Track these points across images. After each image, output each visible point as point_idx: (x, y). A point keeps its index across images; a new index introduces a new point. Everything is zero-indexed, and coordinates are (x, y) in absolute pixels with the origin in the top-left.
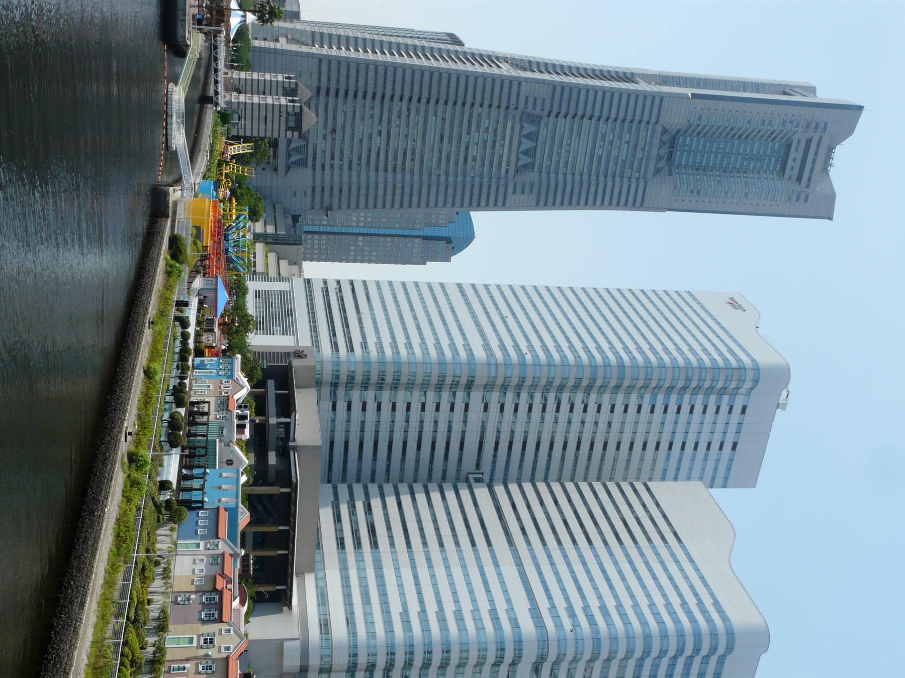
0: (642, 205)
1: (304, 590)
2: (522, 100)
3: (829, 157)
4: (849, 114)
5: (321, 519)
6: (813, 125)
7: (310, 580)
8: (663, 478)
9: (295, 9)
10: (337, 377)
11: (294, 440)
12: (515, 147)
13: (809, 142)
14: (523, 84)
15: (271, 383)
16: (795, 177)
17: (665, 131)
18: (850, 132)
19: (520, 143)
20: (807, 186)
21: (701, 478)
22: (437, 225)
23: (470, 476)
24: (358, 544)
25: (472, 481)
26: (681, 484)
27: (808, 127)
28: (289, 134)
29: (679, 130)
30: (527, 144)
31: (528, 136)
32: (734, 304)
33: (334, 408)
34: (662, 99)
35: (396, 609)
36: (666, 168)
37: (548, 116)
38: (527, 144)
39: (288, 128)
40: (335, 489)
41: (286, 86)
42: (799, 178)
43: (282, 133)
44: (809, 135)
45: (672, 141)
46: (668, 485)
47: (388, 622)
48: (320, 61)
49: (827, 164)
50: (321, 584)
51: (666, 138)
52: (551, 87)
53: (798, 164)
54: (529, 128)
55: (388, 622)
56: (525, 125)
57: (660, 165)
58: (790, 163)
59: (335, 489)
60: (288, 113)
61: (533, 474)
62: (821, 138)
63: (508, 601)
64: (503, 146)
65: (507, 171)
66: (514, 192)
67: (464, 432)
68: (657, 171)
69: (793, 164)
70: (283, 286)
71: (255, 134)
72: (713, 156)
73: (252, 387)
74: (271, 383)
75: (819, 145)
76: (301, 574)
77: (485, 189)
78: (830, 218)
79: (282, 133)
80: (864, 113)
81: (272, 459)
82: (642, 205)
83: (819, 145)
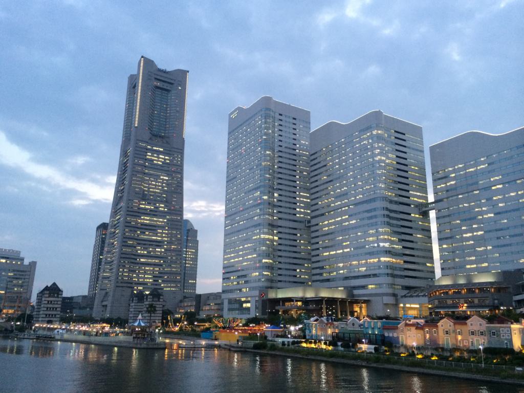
0: (181, 150)
6: (150, 77)
9: (81, 298)
18: (153, 61)
20: (175, 80)
23: (307, 225)
27: (150, 79)
28: (161, 300)
29: (150, 133)
33: (280, 281)
39: (159, 301)
41: (136, 301)
42: (172, 84)
43: (161, 303)
44: (153, 79)
48: (117, 286)
49: (165, 72)
57: (165, 142)
58: (165, 87)
60: (153, 301)
62: (155, 74)
68: (167, 142)
69: (166, 86)
71: (161, 315)
72: (161, 119)
79: (161, 303)
80: (189, 76)
82: (181, 150)
83: (157, 75)
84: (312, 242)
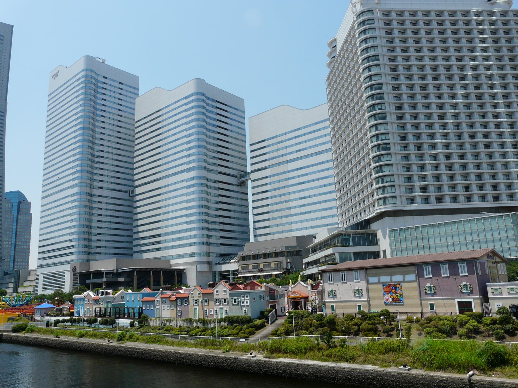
0: (3, 112)
1: (177, 264)
5: (148, 258)
7: (173, 262)
8: (134, 114)
10: (85, 252)
11: (113, 270)
15: (87, 281)
21: (134, 99)
22: (12, 208)
24: (159, 242)
25: (133, 195)
26: (137, 107)
32: (55, 76)
35: (185, 226)
40: (135, 252)
46: (137, 112)
47: (190, 230)
50: (175, 257)
55: (190, 230)
59: (135, 252)
61: (131, 169)
63: (183, 181)
67: (111, 198)
70: (41, 278)
73: (89, 290)
74: (87, 281)
76: (171, 266)
78: (13, 26)
81: (121, 279)
82: (3, 112)
84: (134, 212)
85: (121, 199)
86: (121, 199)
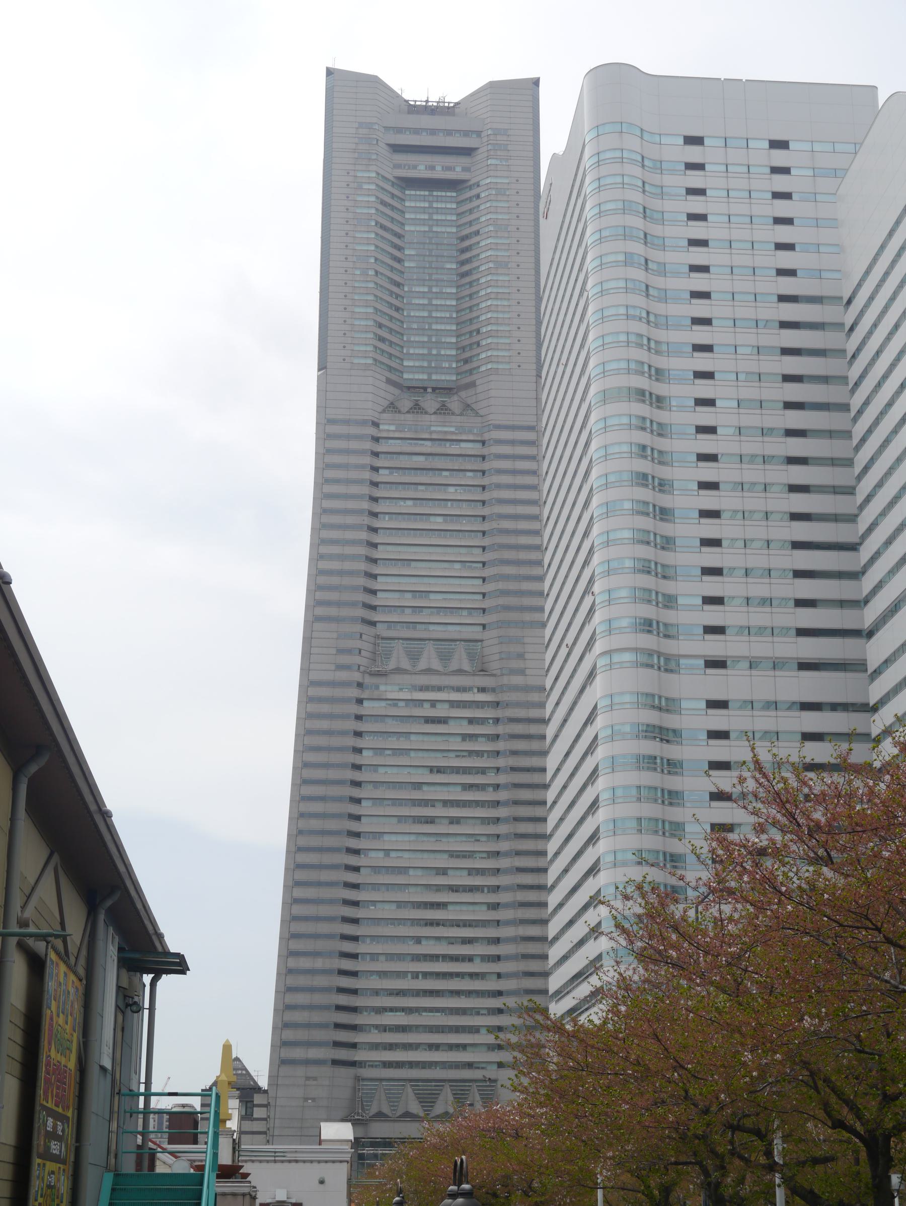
2: (343, 675)
3: (428, 110)
4: (352, 99)
12: (435, 680)
13: (397, 149)
14: (314, 676)
16: (464, 160)
17: (392, 407)
19: (429, 671)
20: (479, 133)
29: (389, 381)
30: (430, 658)
31: (414, 657)
34: (331, 422)
36: (463, 394)
37: (373, 624)
38: (430, 658)
42: (468, 152)
45: (411, 395)
51: (406, 404)
52: (318, 626)
53: (439, 161)
54: (398, 658)
56: (392, 665)
58: (439, 173)
64: (433, 703)
65: (482, 690)
66: (522, 672)
75: (399, 130)
77: (519, 729)
78: (536, 82)
85: (835, 707)
86: (835, 707)
